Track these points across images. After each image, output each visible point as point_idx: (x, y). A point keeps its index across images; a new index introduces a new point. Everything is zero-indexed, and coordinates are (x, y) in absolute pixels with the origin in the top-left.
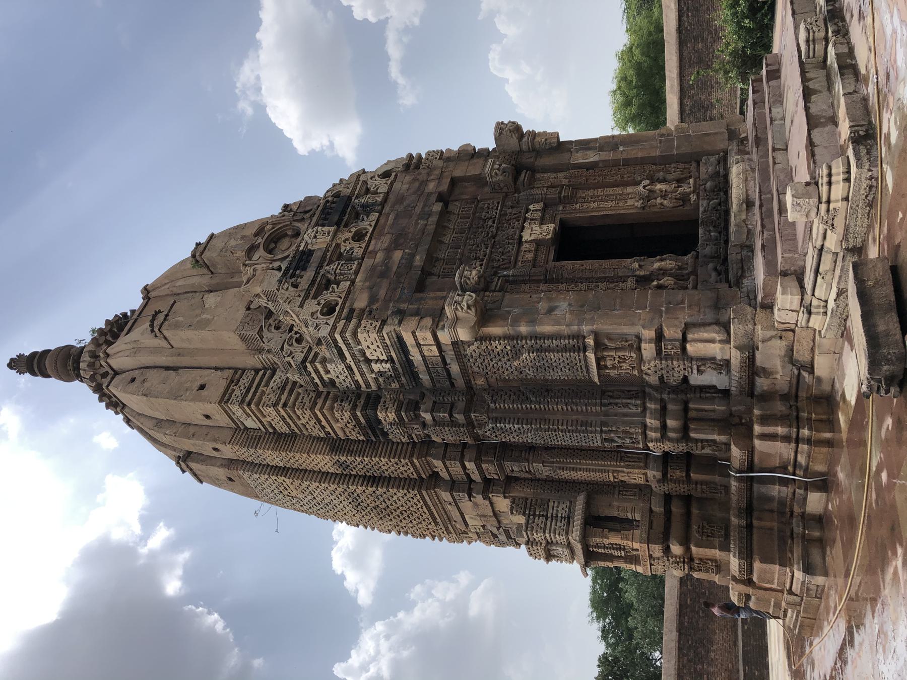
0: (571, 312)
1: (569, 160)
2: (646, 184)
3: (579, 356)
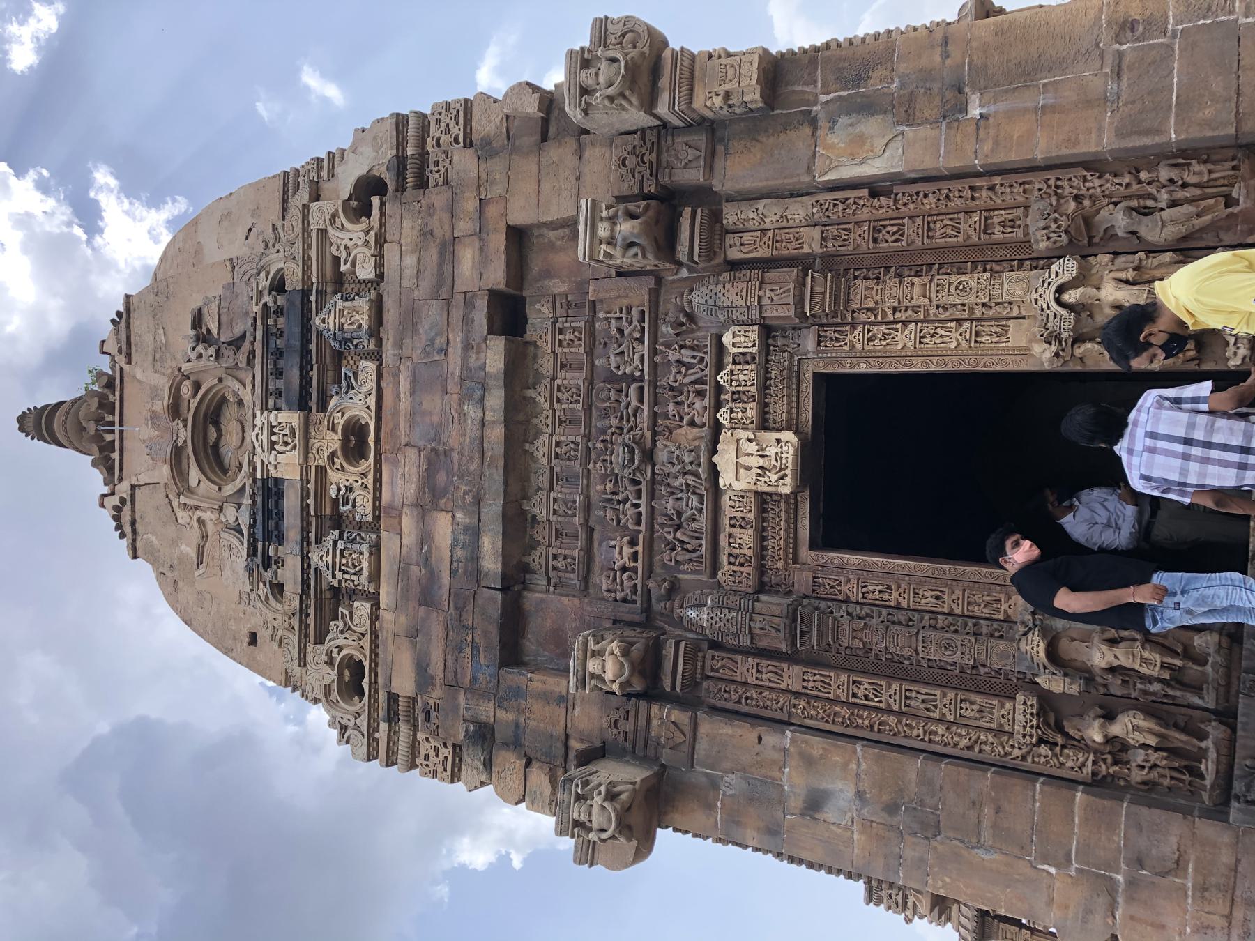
0: (867, 824)
1: (809, 170)
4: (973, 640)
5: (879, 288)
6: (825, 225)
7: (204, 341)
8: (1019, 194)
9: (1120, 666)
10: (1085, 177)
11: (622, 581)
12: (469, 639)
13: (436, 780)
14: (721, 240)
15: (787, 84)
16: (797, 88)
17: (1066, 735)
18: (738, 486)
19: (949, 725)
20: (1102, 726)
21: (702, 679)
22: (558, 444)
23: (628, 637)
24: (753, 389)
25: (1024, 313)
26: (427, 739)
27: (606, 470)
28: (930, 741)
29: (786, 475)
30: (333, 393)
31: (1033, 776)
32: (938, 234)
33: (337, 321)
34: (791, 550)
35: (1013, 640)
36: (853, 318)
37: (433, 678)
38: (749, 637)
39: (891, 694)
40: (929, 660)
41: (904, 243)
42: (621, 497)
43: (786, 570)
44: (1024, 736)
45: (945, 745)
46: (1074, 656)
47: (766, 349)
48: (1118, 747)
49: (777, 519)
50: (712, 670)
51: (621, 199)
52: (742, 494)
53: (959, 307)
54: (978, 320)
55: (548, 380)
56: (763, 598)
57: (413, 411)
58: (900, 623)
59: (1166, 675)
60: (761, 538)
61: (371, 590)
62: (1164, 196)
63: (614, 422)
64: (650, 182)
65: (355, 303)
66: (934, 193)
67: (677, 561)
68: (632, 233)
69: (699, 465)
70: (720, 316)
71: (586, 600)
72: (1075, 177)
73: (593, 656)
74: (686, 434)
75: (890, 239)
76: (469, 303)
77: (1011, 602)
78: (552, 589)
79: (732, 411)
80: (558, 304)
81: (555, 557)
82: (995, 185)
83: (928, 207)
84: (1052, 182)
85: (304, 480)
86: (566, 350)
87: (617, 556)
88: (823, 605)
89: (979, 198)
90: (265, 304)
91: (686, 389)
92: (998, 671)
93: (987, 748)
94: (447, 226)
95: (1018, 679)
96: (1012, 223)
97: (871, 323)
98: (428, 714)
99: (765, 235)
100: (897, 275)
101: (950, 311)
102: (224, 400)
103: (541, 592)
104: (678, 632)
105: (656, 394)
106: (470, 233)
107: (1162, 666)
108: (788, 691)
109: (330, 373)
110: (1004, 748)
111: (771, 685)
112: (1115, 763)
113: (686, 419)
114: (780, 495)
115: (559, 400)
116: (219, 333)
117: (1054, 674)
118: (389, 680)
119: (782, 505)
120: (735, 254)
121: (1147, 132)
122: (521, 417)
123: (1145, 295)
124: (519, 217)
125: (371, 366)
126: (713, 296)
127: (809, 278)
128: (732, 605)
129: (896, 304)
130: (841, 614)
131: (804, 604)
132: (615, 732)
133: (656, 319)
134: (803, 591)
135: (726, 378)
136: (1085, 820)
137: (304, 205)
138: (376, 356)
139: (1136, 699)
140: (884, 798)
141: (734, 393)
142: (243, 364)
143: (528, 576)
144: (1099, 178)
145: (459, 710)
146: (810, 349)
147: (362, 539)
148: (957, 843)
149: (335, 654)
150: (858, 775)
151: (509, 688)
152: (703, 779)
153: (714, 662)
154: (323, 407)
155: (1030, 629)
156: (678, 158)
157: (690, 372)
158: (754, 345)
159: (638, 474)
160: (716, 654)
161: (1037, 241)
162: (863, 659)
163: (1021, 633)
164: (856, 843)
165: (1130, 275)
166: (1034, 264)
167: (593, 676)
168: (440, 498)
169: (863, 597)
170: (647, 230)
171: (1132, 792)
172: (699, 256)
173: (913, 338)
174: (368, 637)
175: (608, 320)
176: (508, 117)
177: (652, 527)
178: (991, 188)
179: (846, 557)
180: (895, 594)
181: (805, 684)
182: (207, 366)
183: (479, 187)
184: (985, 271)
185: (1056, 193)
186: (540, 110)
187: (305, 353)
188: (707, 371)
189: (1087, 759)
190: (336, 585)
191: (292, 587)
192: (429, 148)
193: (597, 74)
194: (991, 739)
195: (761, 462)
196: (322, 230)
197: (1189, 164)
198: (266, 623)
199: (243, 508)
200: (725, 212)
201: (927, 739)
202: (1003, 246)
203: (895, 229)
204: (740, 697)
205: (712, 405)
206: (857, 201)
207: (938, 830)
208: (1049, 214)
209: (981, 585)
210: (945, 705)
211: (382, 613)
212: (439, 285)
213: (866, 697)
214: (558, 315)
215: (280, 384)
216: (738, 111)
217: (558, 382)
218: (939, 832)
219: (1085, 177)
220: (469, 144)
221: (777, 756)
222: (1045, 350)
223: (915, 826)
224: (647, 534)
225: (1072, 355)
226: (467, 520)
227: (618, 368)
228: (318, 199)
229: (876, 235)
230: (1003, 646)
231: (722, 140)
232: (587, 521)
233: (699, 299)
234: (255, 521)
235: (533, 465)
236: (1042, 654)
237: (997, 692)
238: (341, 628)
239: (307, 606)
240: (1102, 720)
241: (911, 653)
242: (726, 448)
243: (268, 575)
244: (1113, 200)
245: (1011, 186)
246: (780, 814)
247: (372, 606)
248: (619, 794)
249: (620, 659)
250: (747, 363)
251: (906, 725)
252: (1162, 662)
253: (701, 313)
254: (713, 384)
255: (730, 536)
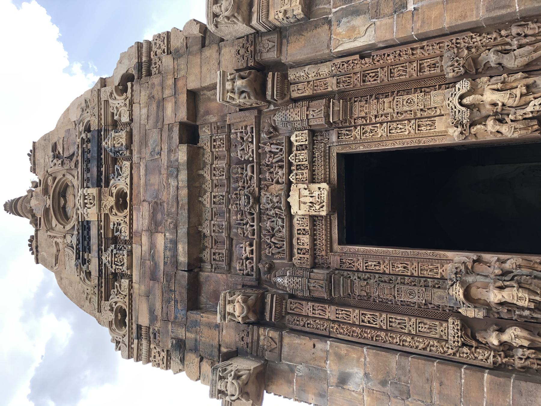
0: (371, 392)
1: (328, 47)
2: (463, 91)
4: (424, 290)
5: (367, 105)
6: (339, 76)
7: (57, 157)
8: (437, 49)
9: (505, 302)
10: (472, 36)
11: (246, 265)
12: (173, 297)
13: (159, 368)
14: (287, 88)
15: (316, 6)
16: (321, 7)
17: (478, 341)
18: (300, 213)
19: (413, 336)
20: (497, 336)
21: (285, 314)
22: (215, 197)
23: (247, 293)
24: (306, 163)
25: (443, 113)
26: (155, 348)
27: (237, 208)
28: (403, 345)
29: (323, 206)
30: (111, 178)
31: (460, 365)
32: (396, 75)
33: (112, 143)
34: (329, 245)
35: (445, 289)
36: (355, 123)
37: (157, 316)
38: (308, 291)
39: (382, 319)
40: (401, 301)
41: (379, 81)
42: (244, 222)
43: (327, 256)
44: (454, 342)
45: (411, 347)
46: (479, 297)
47: (312, 142)
48: (507, 347)
49: (321, 230)
50: (291, 309)
51: (238, 71)
52: (303, 217)
53: (409, 112)
54: (419, 118)
55: (209, 165)
56: (315, 271)
57: (146, 184)
58: (385, 282)
59: (532, 306)
60: (313, 240)
61: (129, 273)
62: (515, 42)
63: (241, 184)
64: (251, 61)
65: (120, 134)
66: (393, 53)
67: (272, 254)
68: (242, 86)
69: (281, 203)
70: (289, 126)
71: (229, 275)
72: (466, 37)
73: (229, 303)
74: (275, 188)
75: (372, 80)
76: (170, 129)
77: (443, 268)
78: (213, 270)
79: (297, 175)
80: (213, 128)
81: (214, 254)
82: (424, 46)
83: (390, 61)
84: (454, 41)
85: (99, 221)
86: (217, 150)
87: (243, 252)
88: (345, 273)
89: (416, 54)
90: (82, 138)
91: (274, 165)
92: (438, 306)
93: (434, 349)
94: (160, 93)
95: (449, 310)
96: (434, 66)
97: (364, 125)
98: (155, 335)
99: (309, 84)
100: (376, 98)
101: (404, 115)
102: (67, 186)
103: (208, 272)
104: (274, 290)
105: (260, 169)
106: (170, 95)
107: (529, 301)
108: (329, 320)
109: (111, 169)
110: (443, 348)
111: (320, 316)
112: (506, 357)
113: (275, 180)
114: (322, 216)
115: (214, 175)
116: (63, 153)
117: (469, 307)
118: (137, 318)
119: (323, 222)
120: (295, 95)
121: (503, 7)
122: (197, 184)
123: (508, 96)
124: (193, 85)
125: (127, 164)
126: (285, 117)
127: (331, 103)
128: (299, 275)
129: (376, 113)
130: (355, 278)
131: (336, 273)
132: (242, 343)
133: (259, 130)
134: (335, 266)
135: (293, 158)
136: (490, 390)
137: (98, 89)
138: (130, 159)
139: (516, 320)
140: (380, 377)
141: (297, 166)
142: (73, 167)
143: (202, 264)
144: (479, 36)
145: (169, 332)
146: (334, 141)
147: (125, 248)
148: (420, 402)
149: (114, 306)
150: (365, 364)
151: (192, 321)
152: (286, 367)
153: (291, 305)
154: (107, 185)
155: (454, 282)
156: (264, 48)
157: (276, 156)
158: (306, 140)
159: (252, 210)
160: (293, 301)
161: (448, 73)
162: (367, 302)
163: (450, 285)
164: (365, 402)
165: (499, 86)
166: (447, 86)
167: (229, 314)
168: (158, 226)
169: (366, 269)
170: (250, 84)
171: (516, 373)
172: (277, 96)
173: (386, 131)
174: (127, 297)
175: (236, 133)
176: (186, 38)
177: (260, 237)
178: (422, 48)
179: (357, 247)
180: (382, 266)
181: (337, 316)
182: (58, 169)
183: (174, 72)
184: (421, 92)
185: (457, 47)
186: (200, 32)
187: (99, 160)
188: (284, 155)
189: (490, 355)
190: (114, 272)
191: (95, 273)
192: (152, 57)
193: (220, 6)
194: (436, 344)
195: (311, 200)
196: (106, 101)
197: (527, 24)
198: (84, 292)
199: (74, 236)
200: (289, 74)
201: (401, 344)
202: (431, 79)
203: (374, 74)
204: (305, 323)
205: (287, 172)
206: (354, 61)
207: (409, 396)
208: (453, 58)
209: (428, 260)
210: (410, 326)
211: (134, 284)
212: (157, 122)
213: (369, 322)
214: (213, 133)
215: (89, 175)
216: (292, 21)
217: (214, 166)
218: (410, 396)
219: (472, 36)
220: (169, 53)
221: (323, 355)
222: (455, 131)
223: (397, 393)
224: (258, 240)
225: (470, 133)
226: (171, 237)
227: (241, 157)
228: (105, 86)
229: (364, 79)
230: (440, 292)
231: (285, 37)
232: (229, 235)
233: (278, 118)
234: (79, 242)
235: (203, 208)
236: (462, 296)
237: (438, 318)
238: (116, 293)
239: (102, 283)
240: (497, 332)
241: (392, 298)
242: (294, 193)
243: (84, 268)
244: (488, 48)
245: (433, 45)
246: (326, 386)
247: (129, 281)
248: (241, 376)
249: (242, 304)
250: (303, 150)
251: (390, 337)
252: (529, 299)
253: (280, 126)
254: (287, 162)
255: (298, 239)
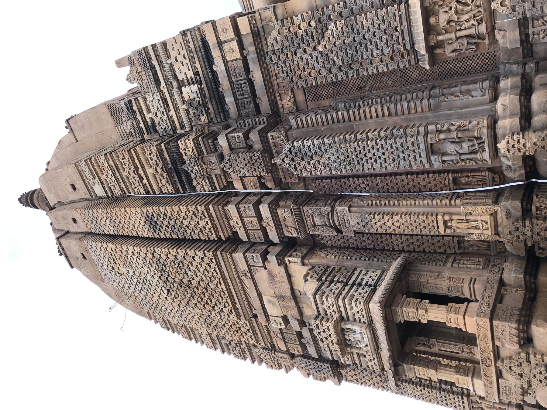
3: (399, 11)
